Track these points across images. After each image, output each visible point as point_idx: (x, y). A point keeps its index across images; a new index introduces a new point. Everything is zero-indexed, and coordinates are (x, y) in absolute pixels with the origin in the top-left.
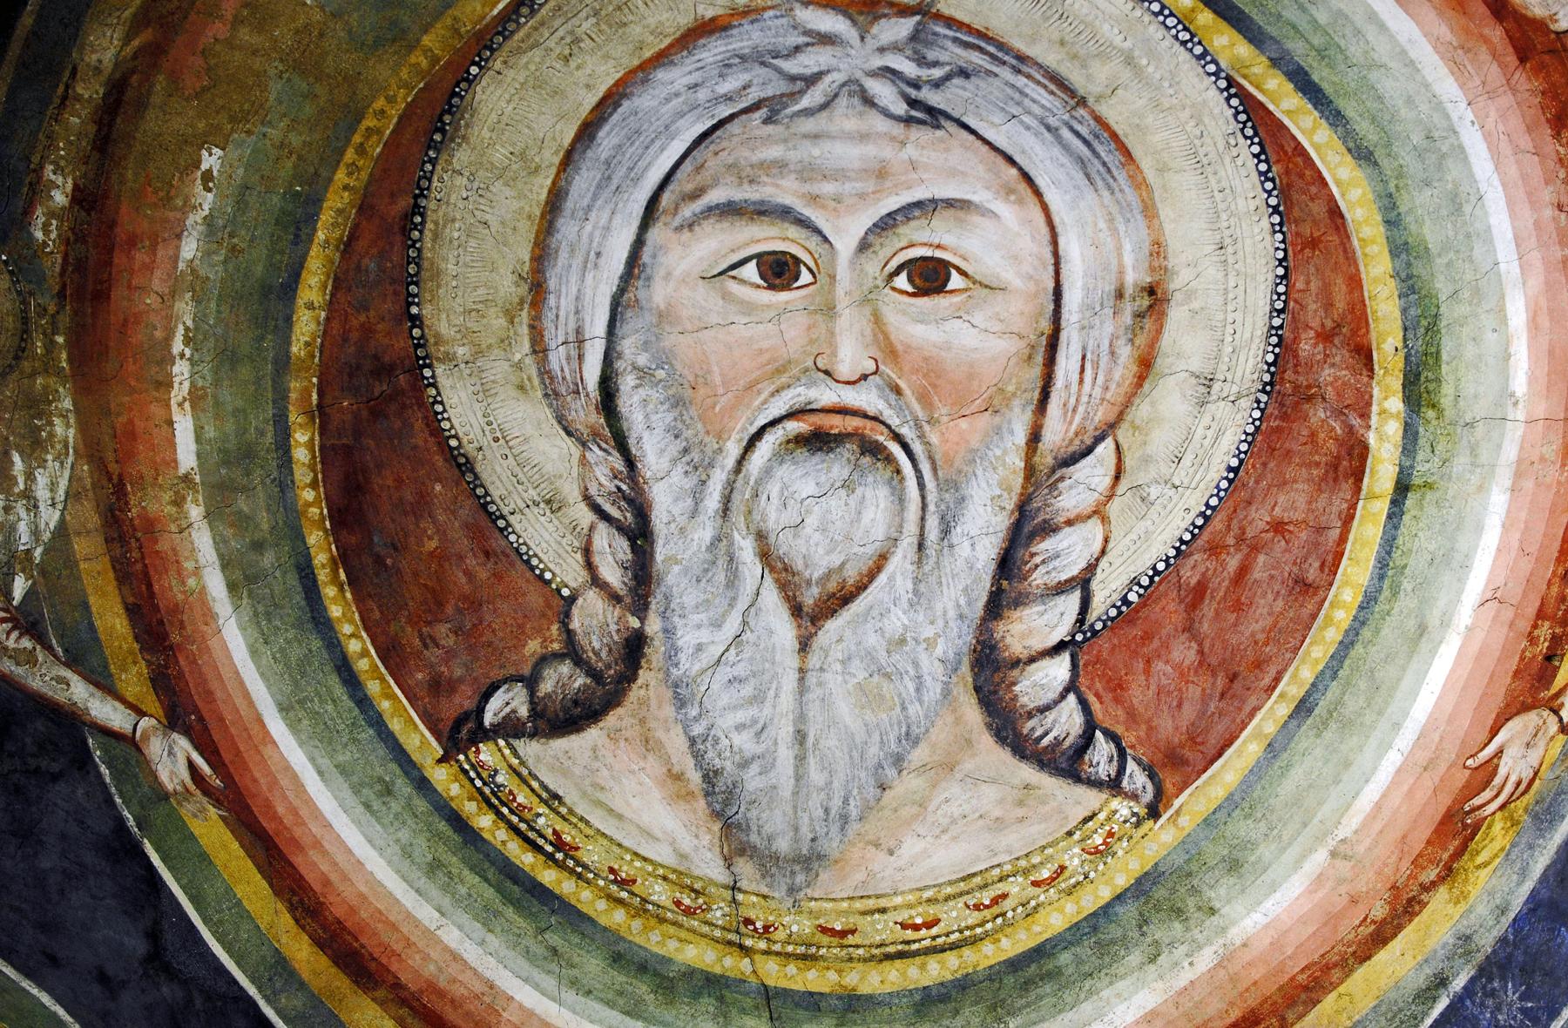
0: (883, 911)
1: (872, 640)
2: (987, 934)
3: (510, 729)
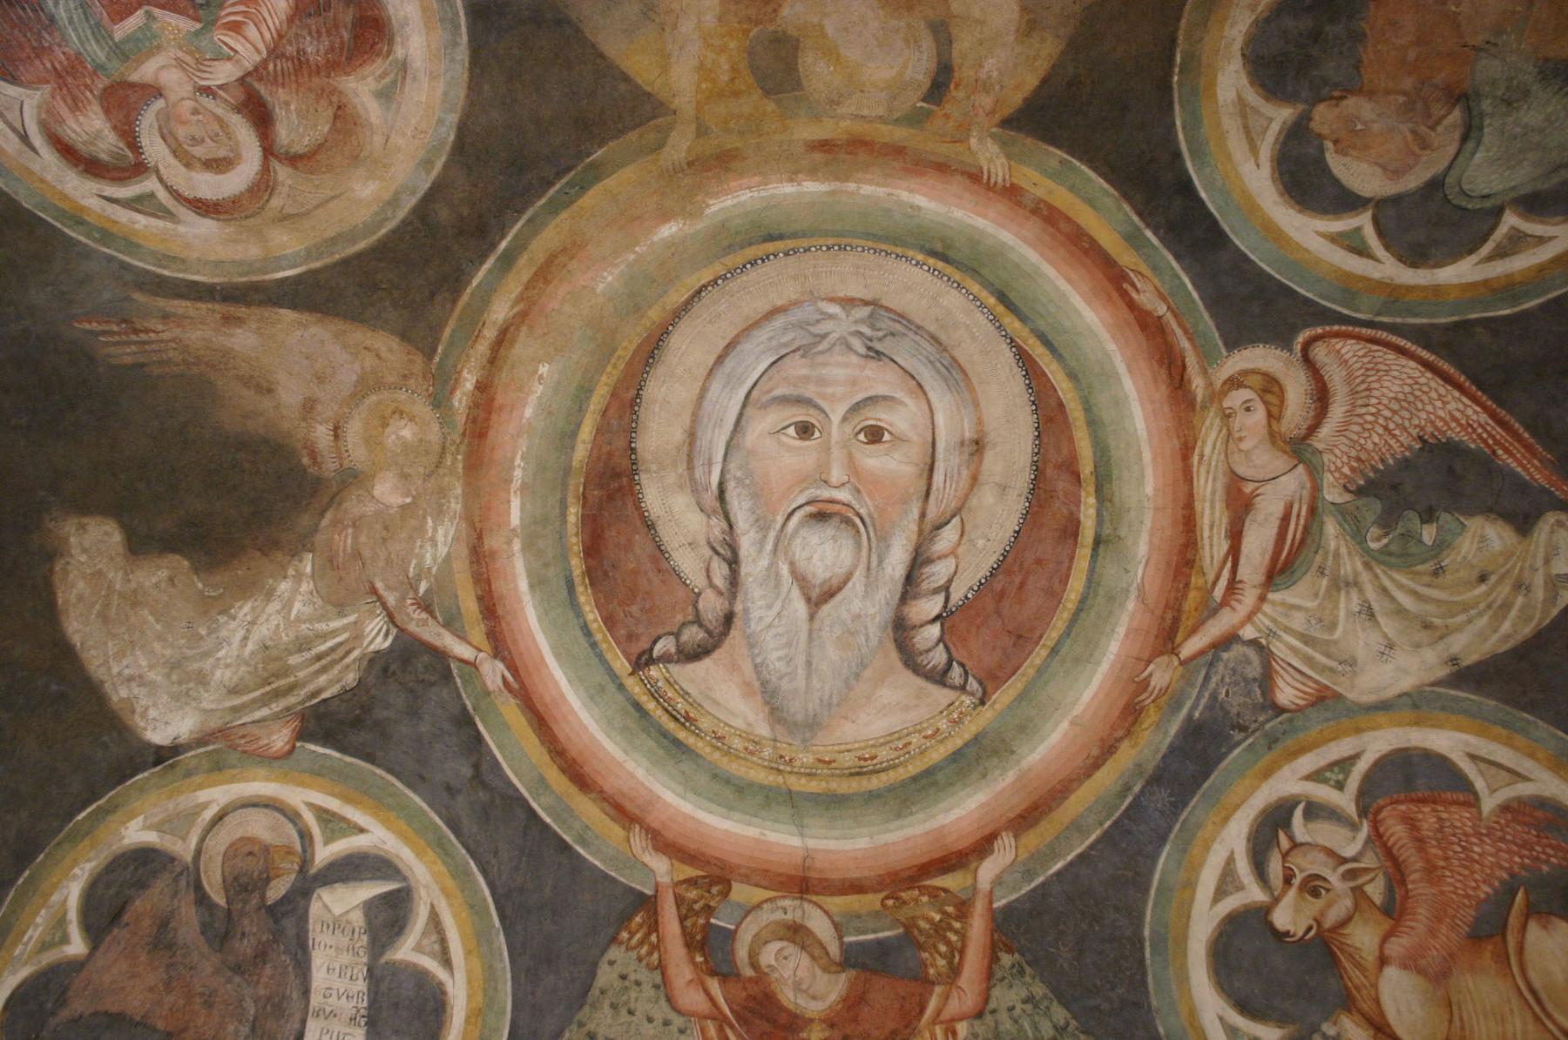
0: (849, 751)
1: (845, 615)
2: (901, 763)
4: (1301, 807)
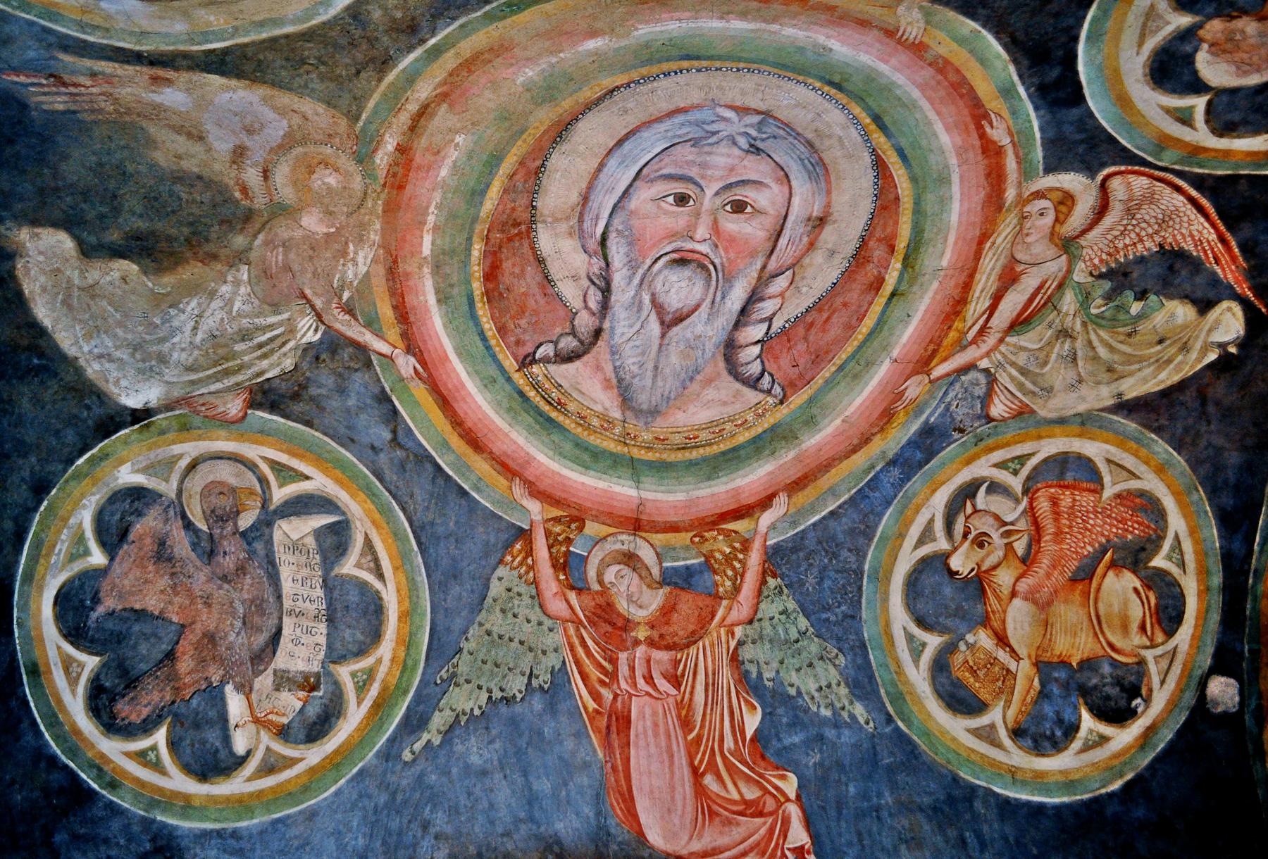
1: (689, 335)
3: (546, 360)
4: (986, 485)
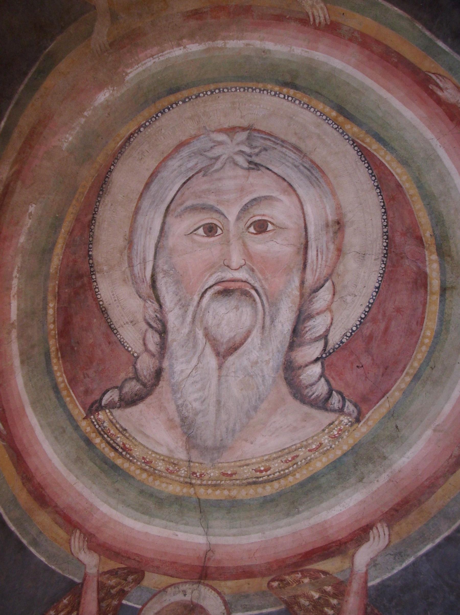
0: (247, 465)
1: (246, 363)
